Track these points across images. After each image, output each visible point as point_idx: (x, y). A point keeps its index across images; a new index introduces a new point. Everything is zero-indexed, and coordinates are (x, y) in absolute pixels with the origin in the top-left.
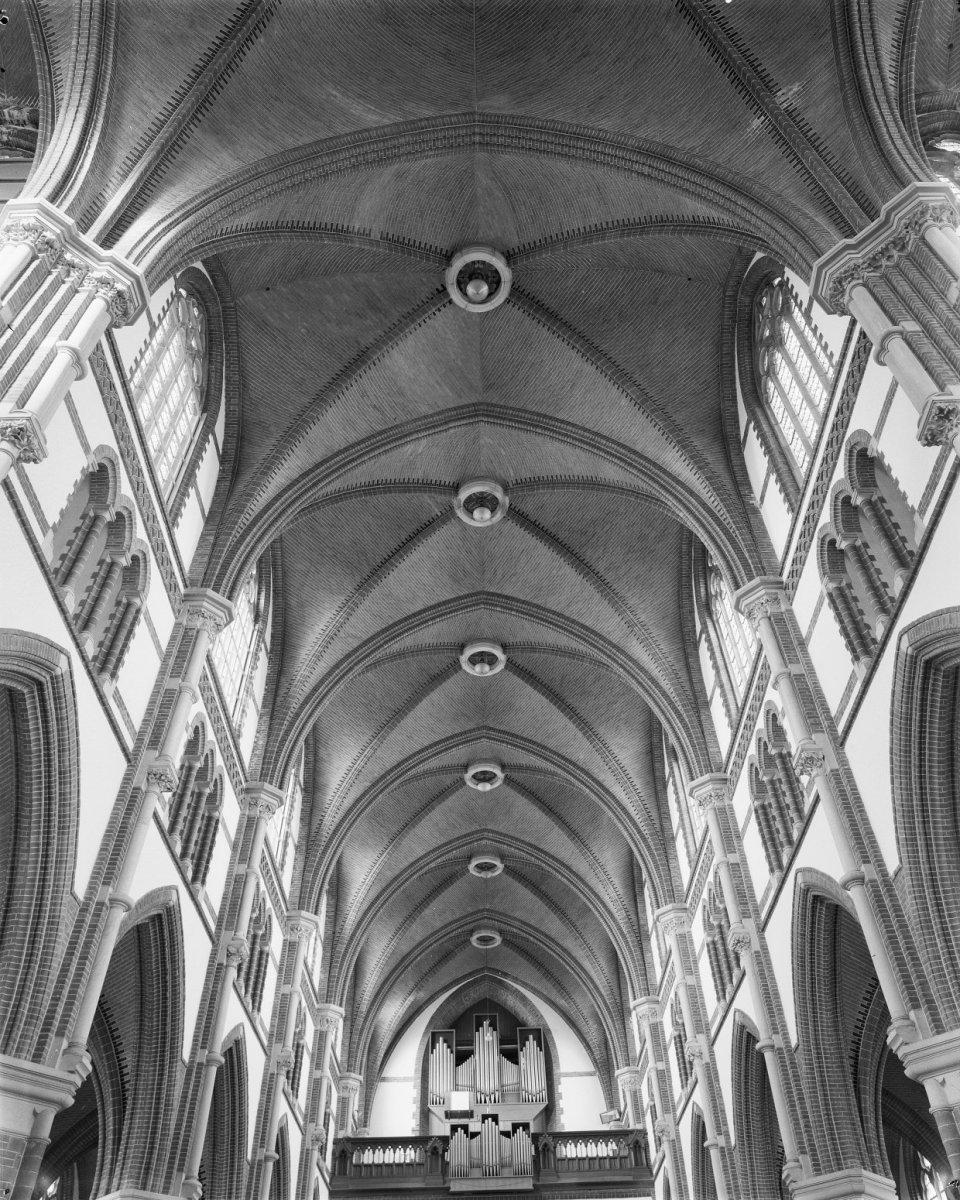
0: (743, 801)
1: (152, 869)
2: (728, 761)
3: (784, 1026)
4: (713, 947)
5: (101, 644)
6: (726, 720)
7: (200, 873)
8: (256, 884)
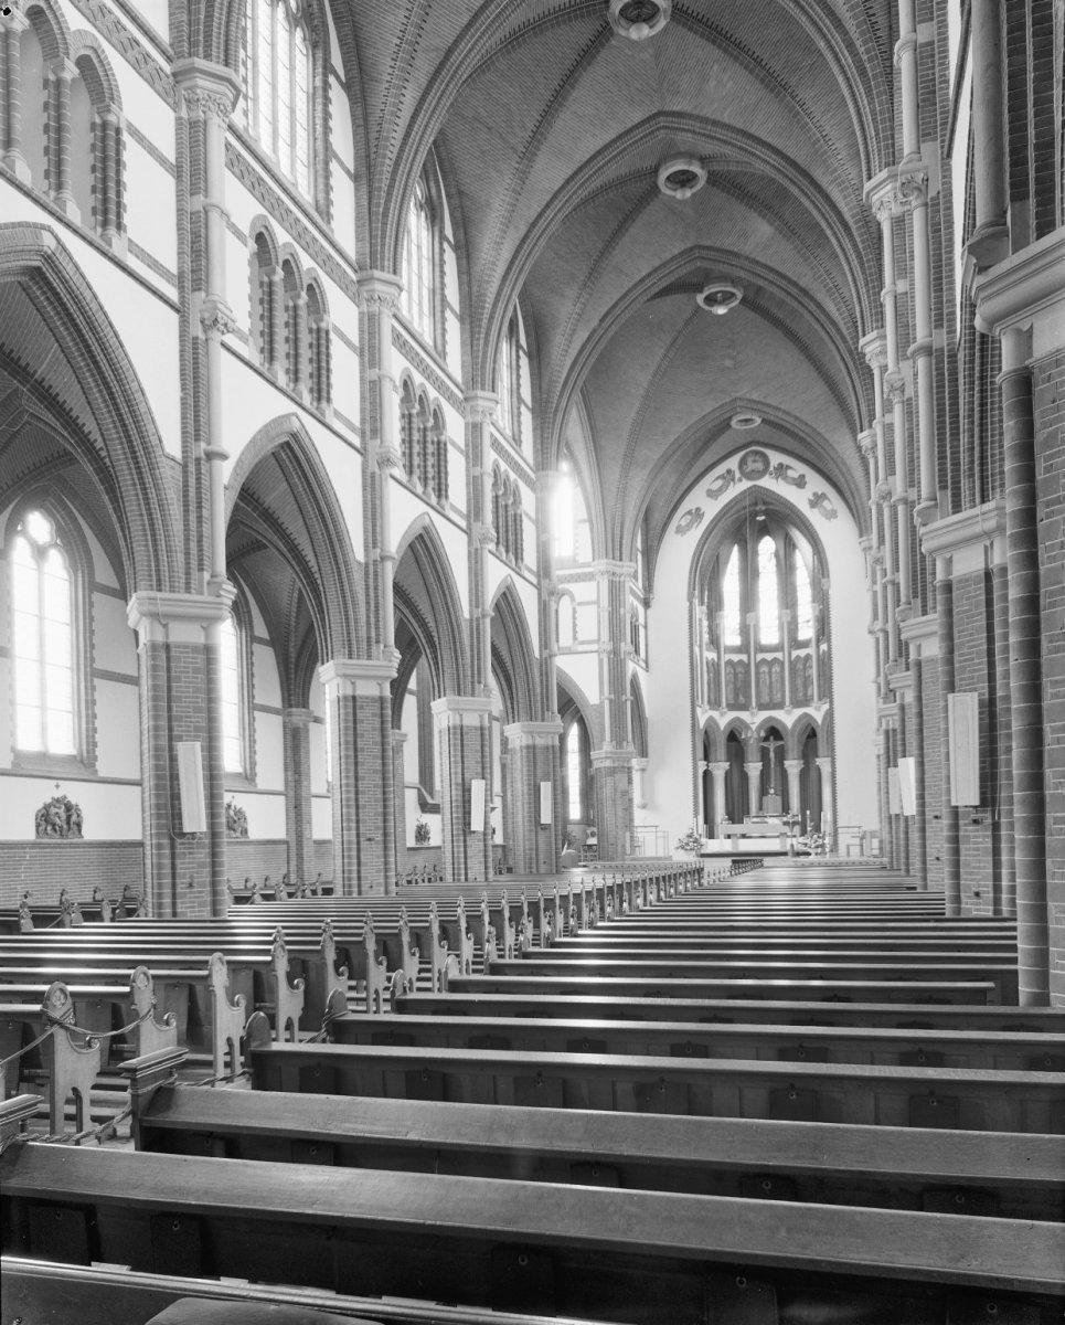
1: (496, 573)
5: (262, 351)
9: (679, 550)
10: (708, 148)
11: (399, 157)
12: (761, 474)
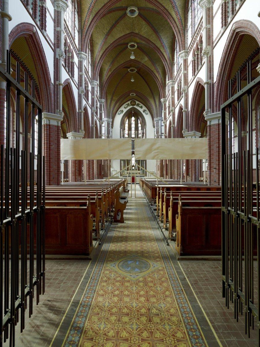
0: (190, 58)
2: (189, 47)
3: (213, 78)
4: (178, 90)
6: (191, 35)
7: (72, 76)
8: (84, 76)
9: (118, 118)
10: (138, 40)
11: (88, 30)
12: (134, 105)
